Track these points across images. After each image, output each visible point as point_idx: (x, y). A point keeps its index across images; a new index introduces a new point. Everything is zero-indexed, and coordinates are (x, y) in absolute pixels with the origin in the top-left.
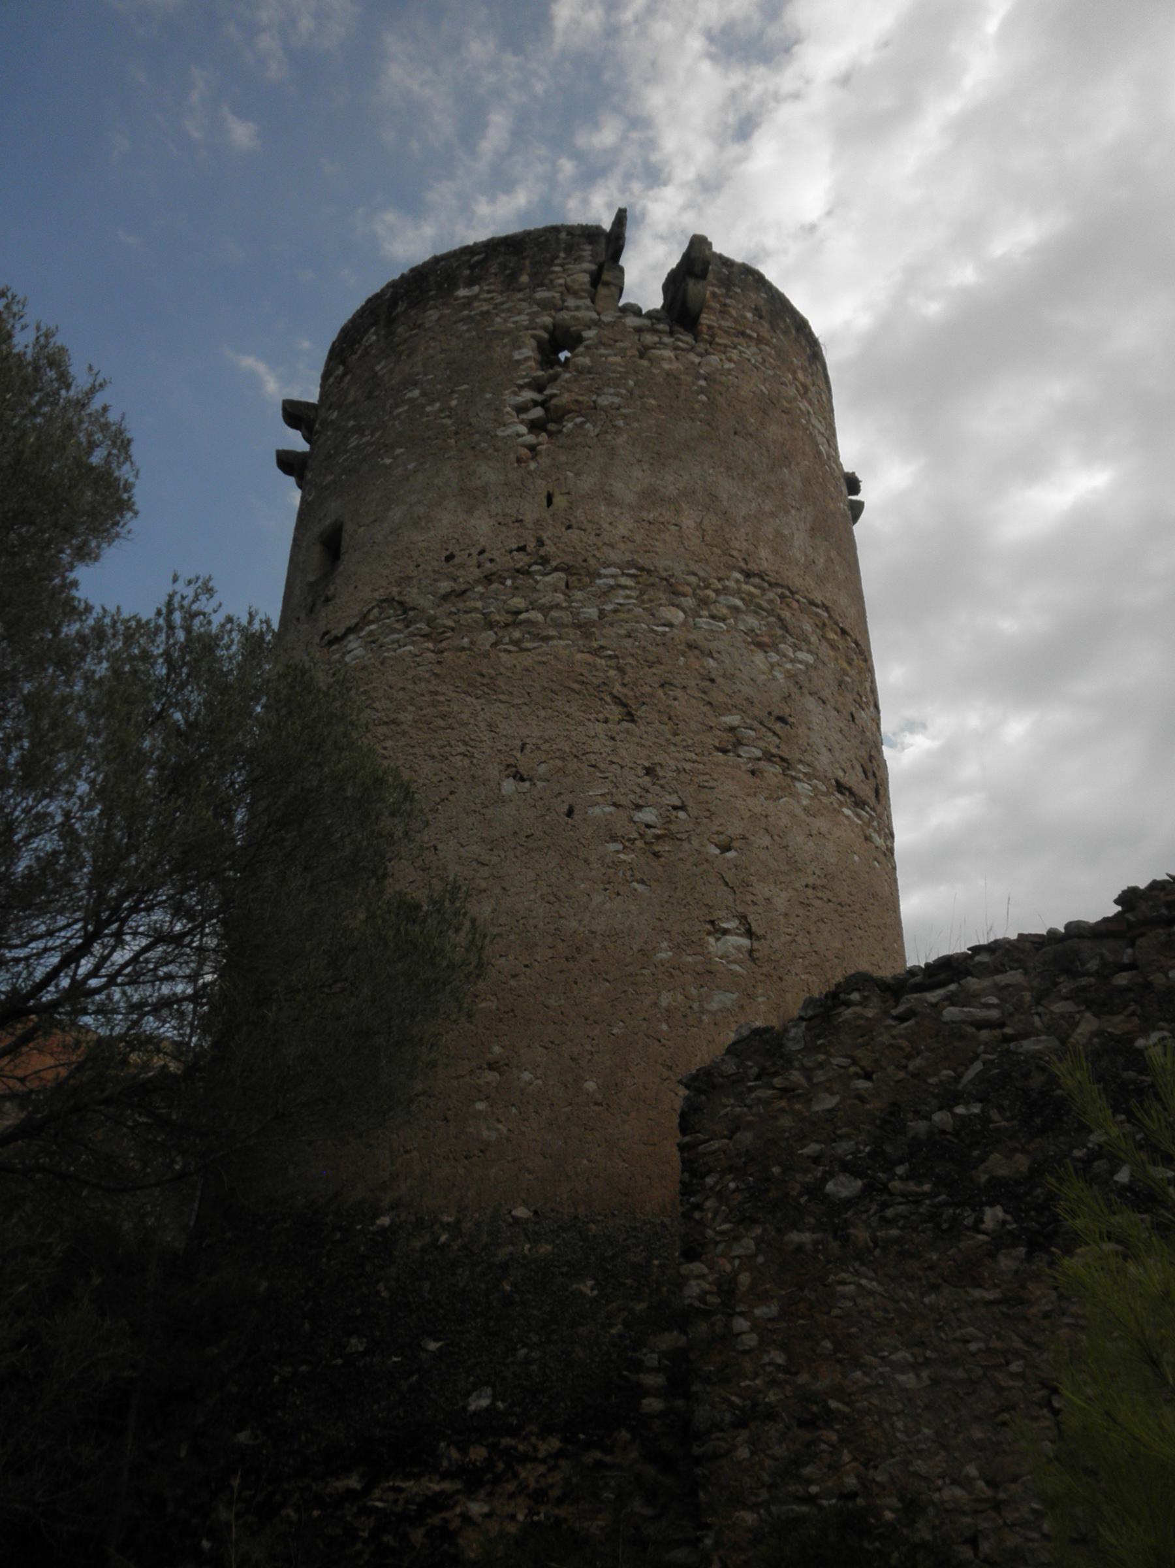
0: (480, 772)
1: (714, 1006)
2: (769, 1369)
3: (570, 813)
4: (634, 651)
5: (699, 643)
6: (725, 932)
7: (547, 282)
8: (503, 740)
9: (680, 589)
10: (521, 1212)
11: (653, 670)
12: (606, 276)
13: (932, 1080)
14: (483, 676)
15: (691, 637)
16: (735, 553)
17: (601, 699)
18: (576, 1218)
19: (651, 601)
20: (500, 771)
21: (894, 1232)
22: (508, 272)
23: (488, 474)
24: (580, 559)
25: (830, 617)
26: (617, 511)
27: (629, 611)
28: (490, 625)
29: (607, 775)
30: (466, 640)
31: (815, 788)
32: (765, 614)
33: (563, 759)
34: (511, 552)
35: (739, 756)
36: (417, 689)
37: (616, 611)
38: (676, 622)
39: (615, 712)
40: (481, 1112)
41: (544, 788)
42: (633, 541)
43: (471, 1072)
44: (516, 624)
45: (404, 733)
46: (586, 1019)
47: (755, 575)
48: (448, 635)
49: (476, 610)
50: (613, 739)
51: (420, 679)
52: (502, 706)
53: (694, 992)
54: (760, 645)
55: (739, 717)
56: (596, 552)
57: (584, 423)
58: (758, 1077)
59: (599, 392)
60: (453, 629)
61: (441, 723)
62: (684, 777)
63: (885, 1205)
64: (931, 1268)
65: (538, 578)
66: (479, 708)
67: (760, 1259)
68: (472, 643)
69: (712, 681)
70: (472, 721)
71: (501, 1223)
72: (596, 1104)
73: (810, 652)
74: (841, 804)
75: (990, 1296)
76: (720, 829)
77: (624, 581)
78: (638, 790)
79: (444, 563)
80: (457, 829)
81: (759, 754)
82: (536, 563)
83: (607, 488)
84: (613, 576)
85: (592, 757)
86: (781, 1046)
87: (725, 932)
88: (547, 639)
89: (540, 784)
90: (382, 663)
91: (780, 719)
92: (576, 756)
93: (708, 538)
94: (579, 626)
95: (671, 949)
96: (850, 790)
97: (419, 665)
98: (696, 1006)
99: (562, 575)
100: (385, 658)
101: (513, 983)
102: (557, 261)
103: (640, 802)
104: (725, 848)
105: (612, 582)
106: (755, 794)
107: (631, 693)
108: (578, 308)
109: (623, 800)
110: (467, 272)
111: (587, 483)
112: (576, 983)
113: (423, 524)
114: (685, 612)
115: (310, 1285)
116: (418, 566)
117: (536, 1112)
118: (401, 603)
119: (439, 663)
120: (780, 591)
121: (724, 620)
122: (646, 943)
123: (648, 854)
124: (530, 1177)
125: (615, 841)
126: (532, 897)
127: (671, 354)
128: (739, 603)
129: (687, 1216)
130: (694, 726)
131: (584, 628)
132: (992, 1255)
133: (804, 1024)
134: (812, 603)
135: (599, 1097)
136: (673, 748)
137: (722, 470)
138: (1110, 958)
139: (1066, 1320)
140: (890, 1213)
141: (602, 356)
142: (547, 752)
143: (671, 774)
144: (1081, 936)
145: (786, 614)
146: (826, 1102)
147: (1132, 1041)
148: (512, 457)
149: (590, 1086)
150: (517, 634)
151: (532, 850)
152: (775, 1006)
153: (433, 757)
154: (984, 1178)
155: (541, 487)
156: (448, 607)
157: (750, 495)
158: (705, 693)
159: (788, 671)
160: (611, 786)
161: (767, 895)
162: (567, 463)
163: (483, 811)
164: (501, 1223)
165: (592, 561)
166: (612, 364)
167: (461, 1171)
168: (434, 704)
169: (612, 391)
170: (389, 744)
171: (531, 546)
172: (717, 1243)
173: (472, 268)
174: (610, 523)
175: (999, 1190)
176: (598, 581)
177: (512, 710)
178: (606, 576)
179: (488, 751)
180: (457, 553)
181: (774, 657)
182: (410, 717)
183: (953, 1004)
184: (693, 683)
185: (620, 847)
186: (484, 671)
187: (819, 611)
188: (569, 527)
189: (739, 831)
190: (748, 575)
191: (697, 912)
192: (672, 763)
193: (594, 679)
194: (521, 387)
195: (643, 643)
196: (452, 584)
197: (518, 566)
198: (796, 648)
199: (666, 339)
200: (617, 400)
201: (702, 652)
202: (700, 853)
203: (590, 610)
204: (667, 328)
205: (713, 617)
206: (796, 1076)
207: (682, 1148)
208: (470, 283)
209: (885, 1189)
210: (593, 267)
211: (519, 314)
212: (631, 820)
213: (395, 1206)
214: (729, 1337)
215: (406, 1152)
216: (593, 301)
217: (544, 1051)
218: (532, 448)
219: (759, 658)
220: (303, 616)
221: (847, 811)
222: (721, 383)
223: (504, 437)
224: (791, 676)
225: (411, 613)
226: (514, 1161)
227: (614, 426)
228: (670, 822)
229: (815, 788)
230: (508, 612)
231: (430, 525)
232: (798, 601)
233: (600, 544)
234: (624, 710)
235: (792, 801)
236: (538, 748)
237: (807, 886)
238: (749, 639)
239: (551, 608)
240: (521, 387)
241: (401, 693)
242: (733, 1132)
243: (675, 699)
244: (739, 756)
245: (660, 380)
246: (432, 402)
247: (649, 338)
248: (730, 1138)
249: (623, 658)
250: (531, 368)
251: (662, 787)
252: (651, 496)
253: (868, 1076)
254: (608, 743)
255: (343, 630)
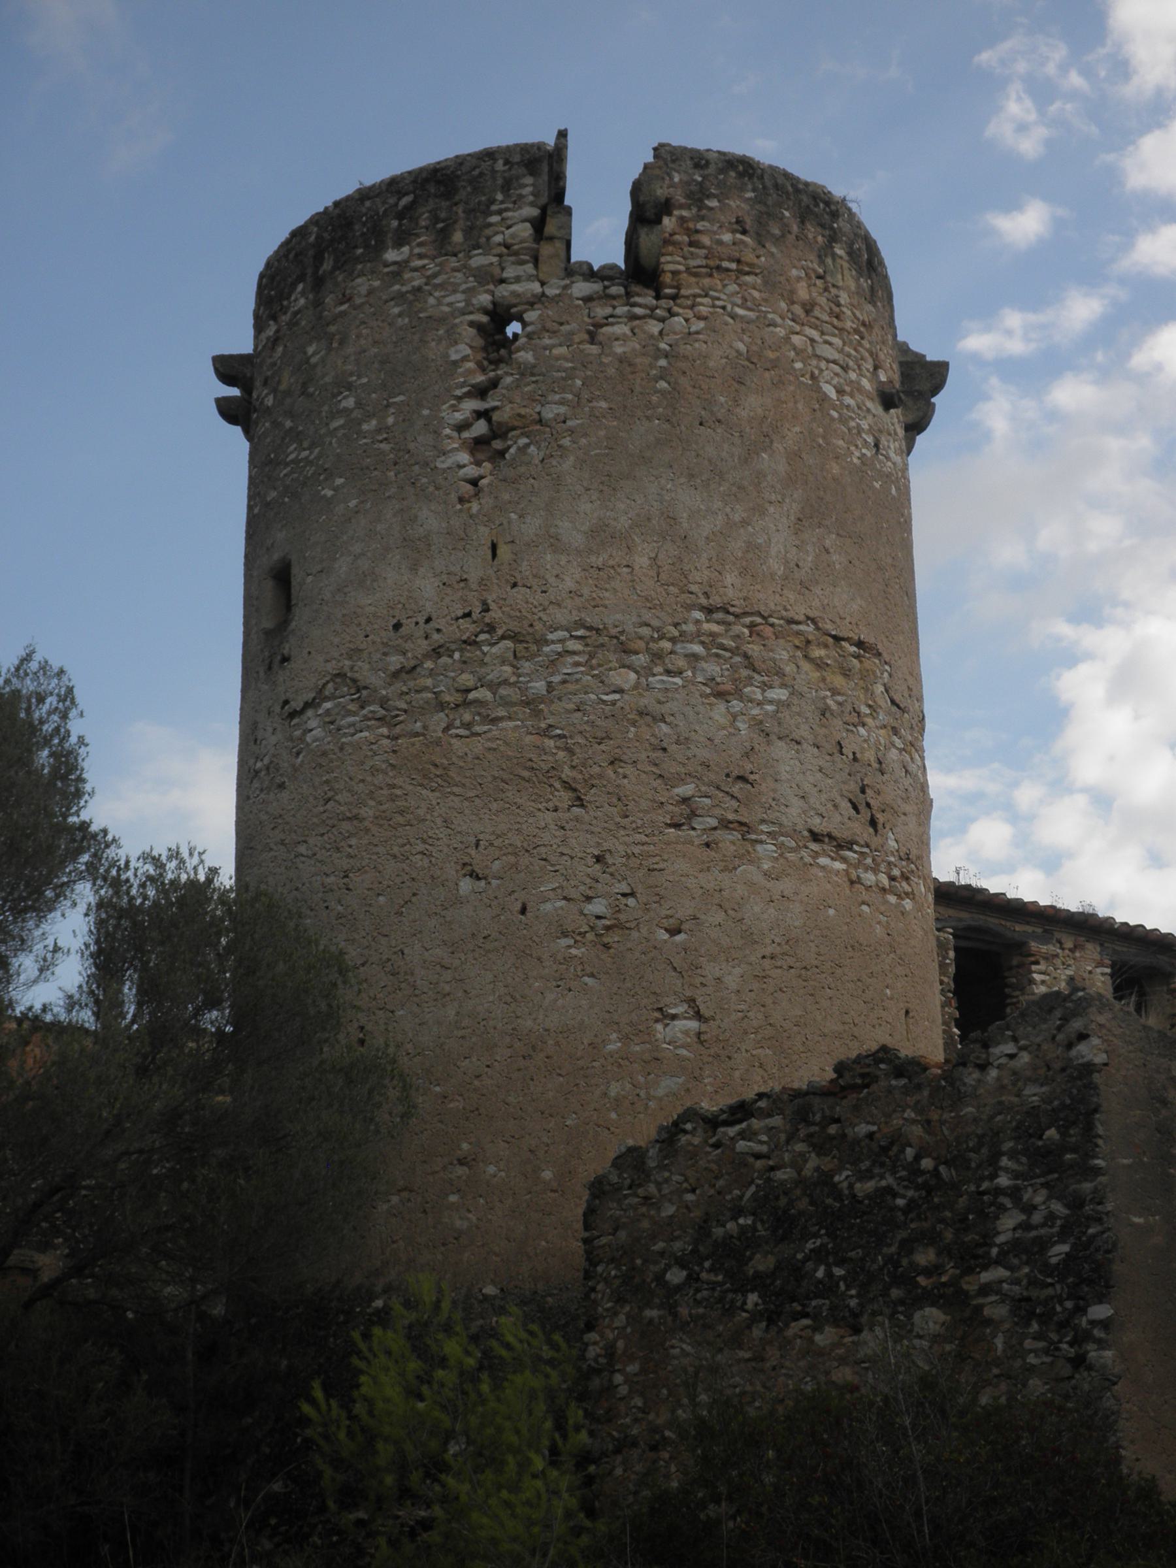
0: (439, 873)
1: (660, 1092)
2: (634, 1410)
3: (523, 911)
4: (581, 728)
5: (650, 709)
6: (674, 1017)
7: (483, 240)
8: (459, 838)
9: (633, 646)
10: (490, 1290)
11: (603, 747)
12: (550, 228)
13: (728, 1197)
14: (436, 766)
15: (644, 702)
16: (693, 588)
17: (551, 786)
18: (536, 1292)
19: (600, 665)
20: (457, 871)
21: (701, 1310)
22: (440, 225)
23: (430, 519)
24: (526, 623)
25: (818, 628)
26: (563, 560)
27: (577, 681)
28: (442, 706)
29: (557, 867)
30: (419, 724)
31: (781, 846)
32: (728, 654)
33: (515, 854)
34: (457, 619)
35: (694, 829)
36: (376, 782)
37: (564, 682)
38: (626, 687)
39: (565, 797)
40: (453, 1203)
41: (499, 887)
42: (582, 596)
43: (444, 1168)
44: (466, 704)
45: (367, 830)
46: (542, 1113)
47: (718, 609)
48: (401, 718)
49: (425, 689)
50: (563, 828)
51: (377, 770)
52: (456, 799)
53: (641, 1079)
54: (720, 695)
55: (693, 786)
56: (541, 614)
57: (527, 445)
58: (630, 1188)
59: (543, 400)
60: (405, 711)
61: (400, 819)
62: (634, 862)
63: (698, 1290)
64: (719, 1336)
65: (486, 649)
66: (434, 802)
67: (629, 1330)
68: (425, 727)
69: (664, 750)
70: (429, 817)
71: (473, 1300)
72: (552, 1191)
73: (783, 686)
74: (816, 855)
75: (748, 1355)
76: (668, 912)
77: (573, 645)
78: (588, 881)
79: (392, 633)
80: (420, 932)
81: (713, 822)
82: (482, 632)
83: (553, 530)
84: (562, 641)
85: (543, 850)
86: (644, 1163)
87: (674, 1017)
88: (495, 721)
89: (494, 882)
90: (341, 749)
91: (741, 778)
92: (527, 851)
93: (663, 576)
94: (527, 703)
95: (620, 1040)
96: (829, 836)
97: (375, 754)
98: (643, 1094)
99: (508, 643)
100: (343, 743)
101: (476, 1083)
102: (494, 208)
103: (590, 893)
104: (674, 932)
105: (558, 647)
106: (708, 869)
107: (580, 776)
108: (518, 279)
109: (573, 894)
110: (395, 223)
111: (531, 527)
112: (532, 1080)
113: (369, 582)
114: (637, 672)
115: (321, 1361)
116: (367, 636)
117: (501, 1201)
118: (354, 681)
119: (394, 752)
120: (748, 620)
121: (680, 673)
122: (596, 1036)
123: (598, 946)
124: (498, 1259)
125: (567, 936)
126: (491, 998)
127: (626, 329)
128: (697, 649)
129: (587, 1296)
130: (644, 805)
131: (531, 703)
132: (749, 1327)
133: (658, 1146)
134: (791, 621)
135: (555, 1185)
136: (622, 832)
137: (683, 480)
138: (828, 1113)
139: (784, 1371)
140: (699, 1296)
141: (545, 349)
142: (501, 849)
143: (620, 860)
144: (814, 1094)
145: (754, 649)
146: (669, 1210)
147: (832, 1177)
148: (453, 497)
149: (547, 1175)
150: (467, 717)
151: (489, 951)
152: (643, 1131)
153: (395, 857)
154: (751, 1272)
155: (484, 534)
156: (399, 686)
157: (718, 504)
158: (656, 765)
159: (754, 718)
160: (561, 879)
161: (717, 975)
162: (510, 502)
163: (443, 913)
164: (473, 1300)
165: (538, 626)
166: (557, 358)
167: (440, 1257)
168: (393, 798)
169: (557, 397)
170: (353, 841)
171: (477, 610)
172: (605, 1317)
173: (400, 216)
174: (557, 576)
175: (759, 1282)
176: (546, 649)
177: (466, 804)
178: (553, 642)
179: (446, 850)
180: (404, 621)
181: (737, 706)
182: (371, 813)
183: (743, 1139)
184: (643, 756)
185: (572, 942)
186: (438, 761)
187: (802, 627)
188: (515, 585)
189: (690, 912)
190: (709, 611)
191: (645, 1001)
192: (621, 848)
193: (542, 765)
194: (459, 399)
195: (592, 717)
196: (401, 659)
197: (464, 638)
198: (765, 686)
199: (622, 310)
200: (562, 410)
201: (654, 718)
202: (648, 940)
203: (537, 685)
204: (621, 290)
205: (668, 672)
206: (652, 1189)
207: (586, 1241)
208: (399, 244)
209: (698, 1279)
210: (535, 212)
211: (455, 291)
212: (581, 913)
213: (388, 1290)
214: (611, 1388)
215: (394, 1242)
216: (536, 266)
217: (507, 1145)
218: (474, 482)
219: (719, 711)
220: (262, 674)
221: (823, 861)
222: (686, 357)
223: (444, 470)
224: (757, 724)
225: (365, 693)
226: (483, 1245)
227: (560, 446)
228: (619, 911)
229: (781, 846)
230: (458, 691)
231: (375, 584)
232: (772, 625)
233: (547, 603)
234: (574, 795)
235: (751, 868)
236: (491, 844)
237: (764, 957)
238: (708, 691)
239: (500, 684)
240: (459, 399)
241: (361, 785)
242: (616, 1229)
243: (625, 777)
244: (694, 829)
245: (611, 371)
246: (369, 416)
247: (601, 311)
248: (614, 1235)
249: (571, 737)
250: (469, 372)
251: (612, 874)
252: (601, 534)
253: (693, 1191)
254: (557, 833)
255: (301, 705)
